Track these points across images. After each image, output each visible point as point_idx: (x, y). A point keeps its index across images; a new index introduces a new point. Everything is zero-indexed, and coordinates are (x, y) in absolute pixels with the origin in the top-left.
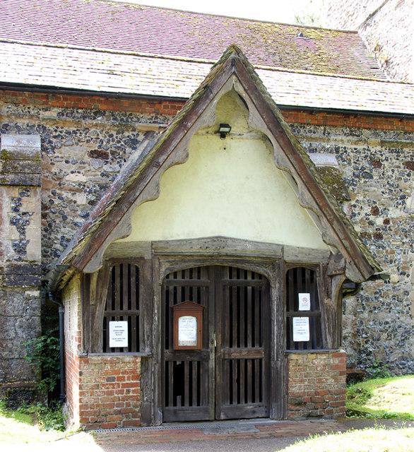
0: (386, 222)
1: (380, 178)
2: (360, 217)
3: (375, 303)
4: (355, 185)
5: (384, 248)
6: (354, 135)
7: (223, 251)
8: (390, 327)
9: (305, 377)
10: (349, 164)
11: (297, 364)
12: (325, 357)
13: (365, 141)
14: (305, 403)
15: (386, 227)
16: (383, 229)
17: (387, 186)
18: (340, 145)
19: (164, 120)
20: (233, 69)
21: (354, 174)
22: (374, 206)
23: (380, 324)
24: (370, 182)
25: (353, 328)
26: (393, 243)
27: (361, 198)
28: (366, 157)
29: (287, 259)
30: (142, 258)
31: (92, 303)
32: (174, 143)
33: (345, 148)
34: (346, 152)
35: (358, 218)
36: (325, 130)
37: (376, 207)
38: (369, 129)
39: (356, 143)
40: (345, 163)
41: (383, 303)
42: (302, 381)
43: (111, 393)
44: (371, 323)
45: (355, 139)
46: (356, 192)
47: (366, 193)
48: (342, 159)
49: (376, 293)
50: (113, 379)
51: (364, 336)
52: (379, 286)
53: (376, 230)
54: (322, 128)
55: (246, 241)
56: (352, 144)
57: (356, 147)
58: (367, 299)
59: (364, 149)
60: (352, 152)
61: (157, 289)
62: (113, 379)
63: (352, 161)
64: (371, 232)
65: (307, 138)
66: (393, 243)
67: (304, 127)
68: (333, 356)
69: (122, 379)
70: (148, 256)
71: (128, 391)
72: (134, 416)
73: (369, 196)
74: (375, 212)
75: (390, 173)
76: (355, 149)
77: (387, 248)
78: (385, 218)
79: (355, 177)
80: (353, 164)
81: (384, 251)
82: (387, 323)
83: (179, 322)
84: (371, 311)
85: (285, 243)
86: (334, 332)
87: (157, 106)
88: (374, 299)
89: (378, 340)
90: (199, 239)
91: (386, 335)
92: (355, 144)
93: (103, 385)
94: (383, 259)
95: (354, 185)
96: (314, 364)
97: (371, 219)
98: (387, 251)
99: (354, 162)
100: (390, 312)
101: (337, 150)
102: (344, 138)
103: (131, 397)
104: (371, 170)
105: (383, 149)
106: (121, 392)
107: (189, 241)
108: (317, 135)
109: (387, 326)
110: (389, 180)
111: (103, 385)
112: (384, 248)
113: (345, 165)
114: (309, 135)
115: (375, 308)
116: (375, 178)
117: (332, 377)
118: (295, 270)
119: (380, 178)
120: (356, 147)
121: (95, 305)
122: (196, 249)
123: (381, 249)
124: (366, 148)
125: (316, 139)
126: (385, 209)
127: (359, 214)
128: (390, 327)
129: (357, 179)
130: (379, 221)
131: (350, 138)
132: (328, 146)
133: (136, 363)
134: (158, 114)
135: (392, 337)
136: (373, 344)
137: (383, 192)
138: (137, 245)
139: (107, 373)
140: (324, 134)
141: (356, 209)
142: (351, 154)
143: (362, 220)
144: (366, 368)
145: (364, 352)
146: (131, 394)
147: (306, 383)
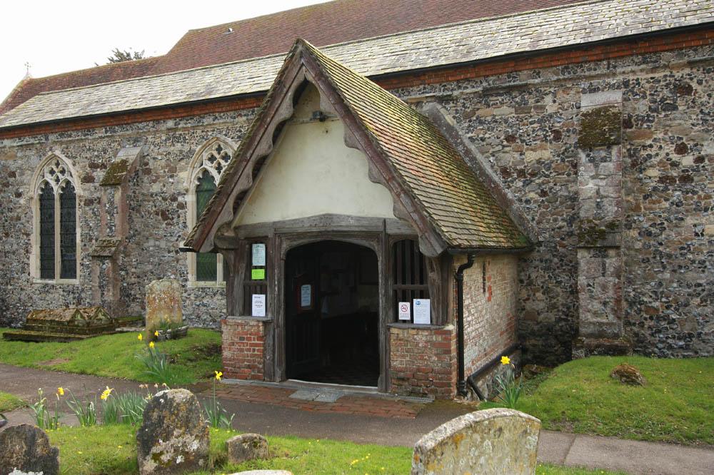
0: (700, 159)
1: (688, 108)
2: (658, 159)
3: (681, 261)
4: (652, 121)
5: (694, 193)
6: (648, 63)
7: (330, 229)
8: (703, 290)
9: (407, 352)
10: (644, 97)
11: (398, 338)
12: (427, 334)
13: (665, 67)
14: (408, 379)
15: (698, 166)
16: (693, 170)
17: (700, 116)
18: (631, 78)
19: (431, 89)
20: (302, 61)
21: (650, 108)
22: (679, 143)
23: (689, 286)
24: (676, 114)
25: (616, 293)
26: (709, 186)
27: (660, 135)
28: (667, 86)
29: (389, 231)
30: (267, 237)
31: (231, 275)
32: (258, 138)
33: (637, 80)
34: (639, 84)
35: (655, 161)
36: (609, 64)
37: (683, 143)
38: (671, 50)
39: (654, 70)
40: (638, 97)
41: (693, 262)
42: (403, 356)
43: (242, 350)
44: (675, 285)
45: (651, 66)
46: (653, 129)
47: (667, 128)
48: (633, 93)
49: (682, 248)
50: (243, 339)
51: (664, 300)
52: (687, 240)
53: (683, 171)
54: (605, 62)
55: (349, 217)
56: (647, 73)
57: (652, 75)
58: (669, 256)
59: (665, 76)
60: (648, 82)
62: (243, 339)
63: (648, 93)
64: (675, 174)
65: (586, 77)
66: (709, 186)
67: (582, 66)
68: (435, 333)
69: (249, 339)
70: (270, 235)
71: (254, 350)
72: (259, 372)
73: (672, 131)
74: (682, 150)
75: (705, 99)
76: (652, 78)
77: (700, 193)
78: (696, 156)
79: (652, 112)
80: (649, 97)
81: (695, 197)
82: (700, 285)
83: (303, 292)
84: (674, 271)
85: (387, 217)
86: (438, 307)
87: (422, 78)
88: (679, 255)
89: (686, 305)
90: (309, 218)
91: (699, 300)
92: (652, 73)
93: (237, 343)
94: (694, 206)
95: (649, 121)
96: (415, 339)
97: (674, 159)
98: (699, 197)
99: (650, 94)
100: (703, 271)
101: (626, 84)
102: (635, 68)
103: (256, 355)
104: (675, 101)
105: (694, 70)
106: (249, 350)
107: (302, 221)
108: (598, 72)
109: (700, 288)
110: (703, 108)
111: (237, 343)
112: (694, 193)
113: (637, 100)
114: (587, 73)
115: (680, 267)
116: (680, 108)
117: (436, 355)
118: (403, 242)
119: (688, 108)
120: (652, 75)
121: (234, 277)
122: (306, 227)
123: (690, 195)
124: (669, 73)
125: (598, 76)
126: (696, 145)
127: (657, 155)
128: (703, 290)
129: (655, 114)
130: (688, 161)
131: (643, 66)
132: (615, 81)
133: (259, 327)
134: (425, 84)
135: (709, 302)
136: (677, 310)
137: (693, 125)
138: (263, 225)
139: (239, 333)
140: (608, 68)
141: (653, 149)
142: (648, 86)
143: (661, 162)
144: (667, 338)
145: (665, 320)
146: (256, 353)
147: (408, 359)
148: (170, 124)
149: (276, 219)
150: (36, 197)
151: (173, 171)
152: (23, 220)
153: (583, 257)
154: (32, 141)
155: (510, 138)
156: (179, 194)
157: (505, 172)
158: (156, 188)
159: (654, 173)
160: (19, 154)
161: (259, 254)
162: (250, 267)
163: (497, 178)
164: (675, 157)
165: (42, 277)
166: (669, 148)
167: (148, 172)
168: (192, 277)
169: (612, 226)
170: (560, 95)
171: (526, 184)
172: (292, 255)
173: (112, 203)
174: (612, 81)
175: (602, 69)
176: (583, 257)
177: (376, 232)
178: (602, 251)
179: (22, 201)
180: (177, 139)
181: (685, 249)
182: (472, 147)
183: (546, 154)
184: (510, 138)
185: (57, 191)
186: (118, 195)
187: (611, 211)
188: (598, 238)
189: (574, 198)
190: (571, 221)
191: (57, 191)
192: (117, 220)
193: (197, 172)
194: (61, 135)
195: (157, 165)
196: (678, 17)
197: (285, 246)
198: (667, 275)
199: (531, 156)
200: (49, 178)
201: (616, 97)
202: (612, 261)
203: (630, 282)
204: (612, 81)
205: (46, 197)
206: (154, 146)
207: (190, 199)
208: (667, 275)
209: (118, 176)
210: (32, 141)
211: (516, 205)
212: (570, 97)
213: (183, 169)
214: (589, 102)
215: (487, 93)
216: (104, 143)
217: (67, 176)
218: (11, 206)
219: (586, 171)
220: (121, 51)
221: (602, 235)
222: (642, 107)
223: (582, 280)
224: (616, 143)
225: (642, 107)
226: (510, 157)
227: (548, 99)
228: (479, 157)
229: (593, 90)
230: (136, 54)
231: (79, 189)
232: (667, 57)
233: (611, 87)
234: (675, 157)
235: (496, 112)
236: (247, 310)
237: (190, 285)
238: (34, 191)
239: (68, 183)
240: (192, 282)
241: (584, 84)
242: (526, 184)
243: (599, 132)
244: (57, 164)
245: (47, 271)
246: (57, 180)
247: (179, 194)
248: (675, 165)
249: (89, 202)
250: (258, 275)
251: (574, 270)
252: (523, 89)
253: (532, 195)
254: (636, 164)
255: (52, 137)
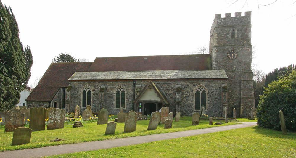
0: (190, 94)
58: (186, 106)
61: (120, 94)
74: (188, 93)
130: (188, 94)
138: (142, 101)
148: (112, 82)
149: (144, 100)
150: (82, 92)
151: (112, 90)
152: (79, 97)
153: (176, 106)
154: (81, 83)
155: (167, 90)
156: (113, 94)
157: (166, 94)
158: (108, 93)
159: (185, 95)
160: (78, 85)
161: (141, 104)
162: (139, 106)
163: (165, 95)
164: (187, 94)
165: (83, 107)
166: (186, 93)
167: (107, 90)
168: (115, 107)
169: (180, 102)
170: (174, 84)
171: (169, 96)
172: (145, 104)
173: (102, 95)
174: (180, 84)
175: (179, 82)
176: (176, 106)
177: (156, 102)
178: (179, 105)
179: (79, 93)
180: (113, 85)
181: (188, 105)
182: (162, 90)
183: (172, 92)
184: (167, 90)
185: (87, 92)
186: (103, 94)
187: (180, 100)
188: (178, 103)
189: (175, 98)
190: (174, 101)
191: (87, 92)
192: (103, 98)
193: (117, 91)
194: (88, 82)
195: (109, 89)
196: (188, 76)
197: (144, 103)
198: (186, 108)
199: (170, 92)
200: (85, 89)
201: (180, 86)
202: (180, 106)
203: (181, 109)
204: (180, 84)
205: (84, 93)
206: (109, 86)
207: (115, 95)
208: (186, 108)
209: (102, 90)
210: (81, 83)
211: (168, 99)
212: (175, 85)
213: (114, 90)
214: (177, 86)
215: (164, 83)
216: (98, 84)
217: (89, 89)
218: (76, 94)
219: (177, 95)
220: (63, 53)
221: (179, 103)
222: (184, 87)
223: (176, 108)
224: (181, 92)
225: (184, 87)
226: (167, 92)
227: (172, 85)
228: (163, 92)
229: (178, 84)
230: (67, 54)
231: (92, 92)
232: (187, 81)
233: (180, 84)
234: (187, 94)
235: (165, 86)
236: (139, 111)
237: (115, 109)
238: (82, 92)
239: (89, 91)
240: (115, 108)
241: (177, 84)
242: (169, 96)
243: (179, 90)
244: (87, 87)
245: (118, 106)
246: (87, 90)
247: (113, 94)
248: (187, 95)
249: (94, 94)
250: (141, 107)
251: (175, 107)
252: (169, 83)
253: (170, 97)
254: (183, 94)
255: (86, 82)
